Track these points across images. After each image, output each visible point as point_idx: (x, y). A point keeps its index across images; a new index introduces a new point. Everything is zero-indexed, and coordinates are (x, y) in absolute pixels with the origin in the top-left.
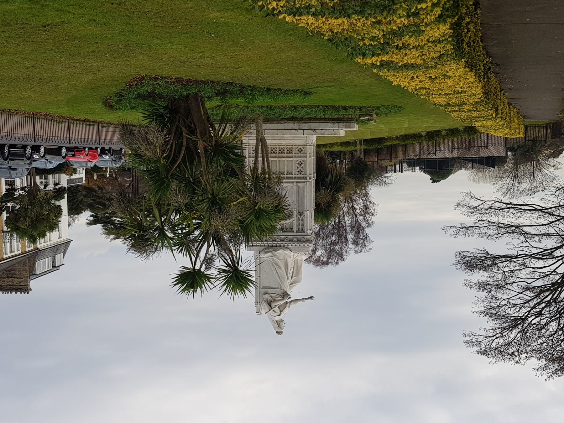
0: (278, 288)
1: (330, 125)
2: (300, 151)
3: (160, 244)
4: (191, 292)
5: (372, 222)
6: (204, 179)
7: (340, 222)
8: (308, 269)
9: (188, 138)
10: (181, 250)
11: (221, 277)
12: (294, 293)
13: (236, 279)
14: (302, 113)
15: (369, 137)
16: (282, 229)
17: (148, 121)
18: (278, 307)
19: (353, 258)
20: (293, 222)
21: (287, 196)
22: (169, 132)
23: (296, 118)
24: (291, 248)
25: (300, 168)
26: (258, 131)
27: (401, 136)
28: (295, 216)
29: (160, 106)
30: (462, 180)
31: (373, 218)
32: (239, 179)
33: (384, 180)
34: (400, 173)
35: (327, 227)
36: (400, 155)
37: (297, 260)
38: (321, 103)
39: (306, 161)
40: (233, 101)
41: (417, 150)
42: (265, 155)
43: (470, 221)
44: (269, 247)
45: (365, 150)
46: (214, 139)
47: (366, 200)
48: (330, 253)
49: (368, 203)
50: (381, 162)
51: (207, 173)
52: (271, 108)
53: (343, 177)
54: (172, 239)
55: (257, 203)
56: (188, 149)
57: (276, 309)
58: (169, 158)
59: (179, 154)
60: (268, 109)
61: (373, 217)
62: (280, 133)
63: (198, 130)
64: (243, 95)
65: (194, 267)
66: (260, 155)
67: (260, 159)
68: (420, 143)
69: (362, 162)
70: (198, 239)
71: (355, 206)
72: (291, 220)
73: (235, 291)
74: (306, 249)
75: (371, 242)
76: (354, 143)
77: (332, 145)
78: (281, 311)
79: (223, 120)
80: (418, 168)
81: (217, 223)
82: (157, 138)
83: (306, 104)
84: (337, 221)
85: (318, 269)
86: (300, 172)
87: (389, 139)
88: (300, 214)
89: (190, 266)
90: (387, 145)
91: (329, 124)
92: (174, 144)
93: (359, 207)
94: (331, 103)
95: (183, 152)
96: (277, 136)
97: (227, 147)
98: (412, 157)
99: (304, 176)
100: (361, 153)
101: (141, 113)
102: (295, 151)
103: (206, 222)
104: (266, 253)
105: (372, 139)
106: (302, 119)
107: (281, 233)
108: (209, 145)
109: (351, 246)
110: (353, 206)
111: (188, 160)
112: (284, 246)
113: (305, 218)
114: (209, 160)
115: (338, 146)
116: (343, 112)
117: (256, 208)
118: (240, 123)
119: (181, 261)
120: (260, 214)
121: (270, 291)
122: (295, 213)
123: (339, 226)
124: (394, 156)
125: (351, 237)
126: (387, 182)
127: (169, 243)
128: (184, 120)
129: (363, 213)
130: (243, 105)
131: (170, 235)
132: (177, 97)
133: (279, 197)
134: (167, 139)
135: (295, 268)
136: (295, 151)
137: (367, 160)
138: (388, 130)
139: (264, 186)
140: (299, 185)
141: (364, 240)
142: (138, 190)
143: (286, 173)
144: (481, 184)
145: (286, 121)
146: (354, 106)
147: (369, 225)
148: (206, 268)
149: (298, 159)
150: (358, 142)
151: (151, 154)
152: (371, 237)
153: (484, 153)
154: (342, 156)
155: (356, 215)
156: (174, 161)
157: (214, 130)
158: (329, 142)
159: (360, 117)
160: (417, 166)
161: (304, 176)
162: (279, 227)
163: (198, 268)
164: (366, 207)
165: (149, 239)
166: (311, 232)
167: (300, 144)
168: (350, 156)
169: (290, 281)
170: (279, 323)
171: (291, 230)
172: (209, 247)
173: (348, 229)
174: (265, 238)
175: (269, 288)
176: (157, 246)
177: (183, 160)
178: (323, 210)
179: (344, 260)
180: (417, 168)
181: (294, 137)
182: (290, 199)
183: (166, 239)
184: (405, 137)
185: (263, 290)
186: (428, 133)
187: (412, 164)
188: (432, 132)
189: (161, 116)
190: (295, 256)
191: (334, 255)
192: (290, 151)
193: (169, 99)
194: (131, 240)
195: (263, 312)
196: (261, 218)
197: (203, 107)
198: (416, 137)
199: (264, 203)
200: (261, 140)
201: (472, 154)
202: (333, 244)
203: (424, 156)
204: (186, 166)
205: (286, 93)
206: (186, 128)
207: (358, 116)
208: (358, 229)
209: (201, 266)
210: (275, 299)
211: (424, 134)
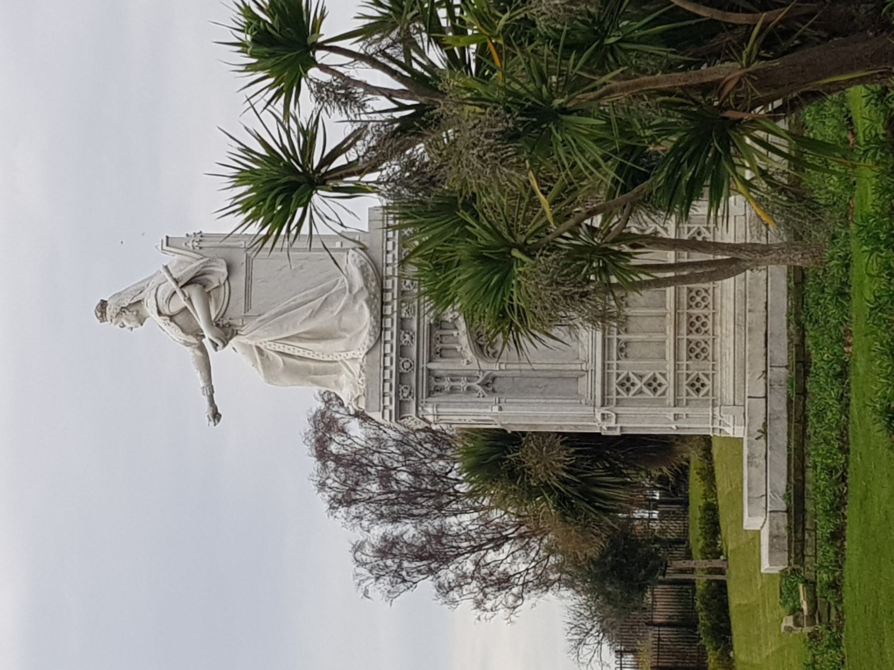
0: (248, 306)
1: (781, 484)
2: (696, 385)
4: (242, 36)
5: (454, 602)
6: (615, 83)
8: (307, 399)
9: (750, 27)
12: (232, 361)
13: (282, 185)
14: (823, 393)
15: (735, 600)
18: (185, 309)
19: (336, 539)
20: (465, 358)
21: (550, 342)
23: (807, 373)
24: (377, 354)
25: (639, 384)
26: (765, 250)
28: (484, 365)
31: (467, 604)
32: (611, 194)
33: (591, 640)
35: (441, 457)
37: (338, 371)
38: (855, 458)
39: (661, 403)
42: (685, 274)
44: (381, 280)
46: (746, 116)
47: (525, 584)
48: (354, 465)
49: (515, 590)
50: (651, 634)
51: (634, 93)
52: (842, 294)
55: (532, 257)
56: (713, 28)
57: (180, 302)
60: (837, 285)
62: (756, 318)
63: (777, 63)
65: (321, 46)
66: (685, 257)
67: (670, 257)
69: (654, 571)
71: (507, 547)
72: (469, 354)
73: (241, 178)
76: (713, 550)
77: (709, 475)
78: (171, 317)
81: (466, 122)
83: (854, 409)
86: (626, 384)
88: (489, 384)
90: (704, 655)
91: (784, 483)
94: (855, 492)
96: (744, 316)
97: (717, 157)
99: (614, 396)
100: (682, 571)
102: (697, 368)
103: (469, 90)
104: (363, 270)
106: (803, 393)
107: (428, 319)
108: (728, 96)
109: (380, 530)
110: (507, 538)
111: (675, 29)
112: (383, 329)
113: (474, 397)
114: (673, 99)
115: (705, 496)
116: (825, 528)
117: (516, 253)
118: (793, 200)
120: (496, 262)
121: (239, 281)
122: (491, 367)
123: (440, 494)
125: (408, 530)
126: (584, 650)
129: (484, 571)
130: (855, 202)
133: (545, 321)
135: (312, 364)
136: (697, 368)
138: (757, 661)
140: (583, 381)
141: (397, 574)
145: (796, 340)
146: (846, 567)
147: (444, 590)
148: (320, 86)
149: (671, 376)
150: (716, 564)
152: (406, 596)
154: (674, 508)
155: (480, 547)
157: (775, 116)
158: (717, 468)
159: (806, 582)
166: (430, 418)
167: (718, 383)
169: (269, 347)
171: (436, 353)
172: (389, 94)
173: (433, 525)
174: (412, 270)
175: (249, 279)
178: (499, 456)
179: (332, 507)
181: (741, 368)
182: (538, 353)
185: (240, 258)
190: (351, 364)
191: (349, 475)
192: (696, 352)
195: (171, 259)
196: (478, 257)
199: (529, 278)
200: (734, 261)
202: (386, 476)
204: (657, 21)
206: (781, 21)
208: (434, 554)
209: (324, 68)
210: (209, 299)
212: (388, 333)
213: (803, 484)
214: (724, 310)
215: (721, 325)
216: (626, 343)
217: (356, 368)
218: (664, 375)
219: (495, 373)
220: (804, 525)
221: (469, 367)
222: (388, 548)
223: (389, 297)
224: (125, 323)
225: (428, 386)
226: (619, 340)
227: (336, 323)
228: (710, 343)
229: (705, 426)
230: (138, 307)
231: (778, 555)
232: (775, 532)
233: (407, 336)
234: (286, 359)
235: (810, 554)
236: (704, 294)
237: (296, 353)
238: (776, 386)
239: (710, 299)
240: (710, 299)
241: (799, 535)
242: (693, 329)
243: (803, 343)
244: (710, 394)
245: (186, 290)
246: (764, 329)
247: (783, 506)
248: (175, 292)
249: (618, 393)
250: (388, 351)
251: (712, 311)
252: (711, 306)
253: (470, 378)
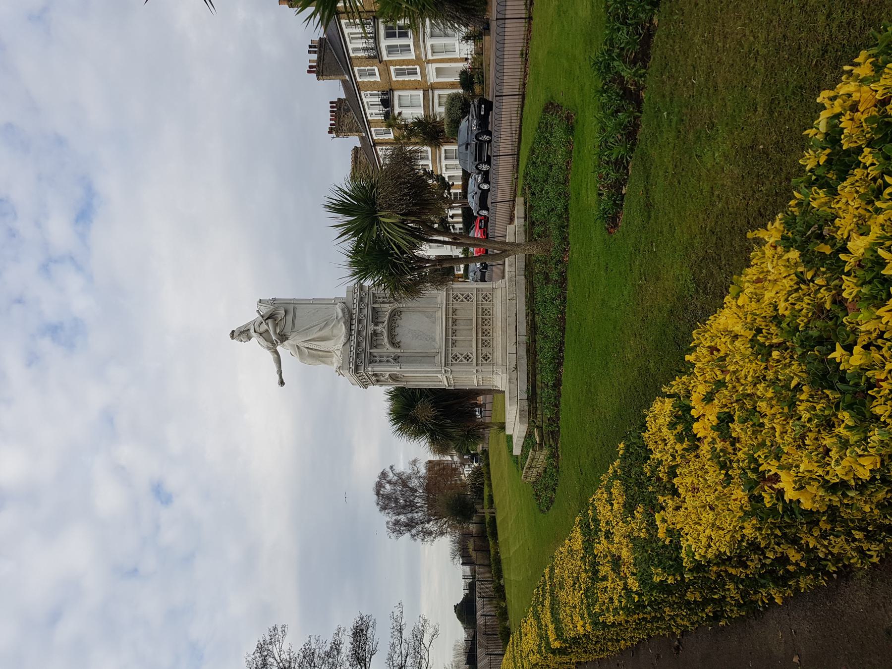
0: (293, 327)
2: (485, 358)
15: (498, 522)
24: (348, 346)
30: (455, 634)
31: (419, 540)
37: (332, 357)
39: (470, 365)
43: (407, 634)
50: (472, 540)
57: (264, 327)
72: (388, 346)
75: (397, 537)
77: (490, 486)
78: (261, 334)
85: (373, 485)
86: (455, 357)
88: (396, 359)
93: (431, 526)
102: (486, 351)
104: (343, 310)
106: (534, 341)
109: (394, 518)
112: (351, 335)
121: (290, 318)
124: (479, 553)
125: (403, 518)
135: (321, 353)
136: (486, 351)
140: (437, 358)
143: (454, 338)
144: (453, 653)
145: (530, 318)
147: (413, 536)
149: (475, 354)
153: (480, 652)
164: (430, 533)
173: (410, 516)
175: (294, 316)
180: (467, 592)
184: (498, 561)
186: (503, 586)
187: (472, 587)
188: (503, 591)
192: (485, 344)
198: (499, 574)
201: (480, 639)
208: (410, 525)
211: (502, 582)
217: (339, 353)
222: (397, 523)
223: (354, 322)
247: (525, 396)
253: (388, 356)
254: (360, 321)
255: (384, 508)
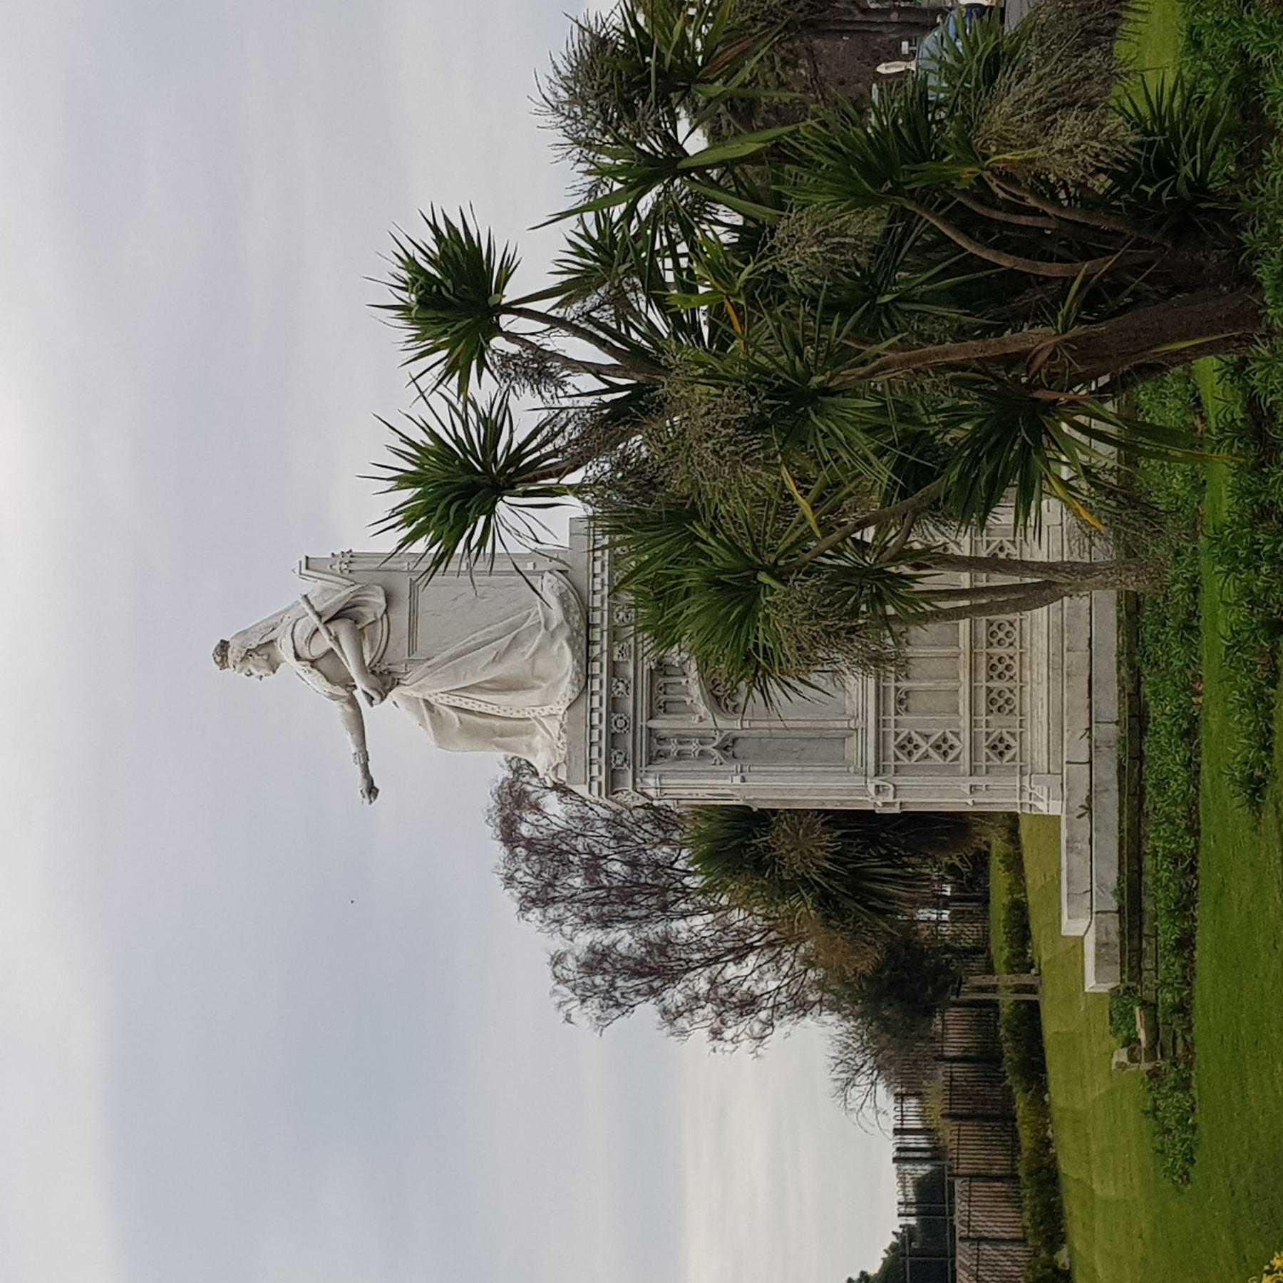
0: (412, 648)
1: (1112, 877)
2: (999, 747)
3: (608, 160)
4: (404, 295)
5: (683, 1032)
6: (891, 355)
7: (685, 892)
9: (1067, 281)
10: (582, 252)
11: (465, 425)
12: (392, 719)
13: (457, 488)
14: (1165, 757)
15: (1051, 1026)
16: (662, 668)
17: (1144, 109)
19: (530, 949)
20: (696, 713)
22: (1089, 201)
24: (582, 709)
25: (925, 747)
26: (1088, 570)
27: (1054, 1160)
28: (721, 723)
29: (1208, 161)
31: (701, 1034)
33: (862, 1080)
34: (891, 1152)
35: (664, 841)
36: (968, 1149)
37: (531, 732)
38: (1208, 843)
39: (953, 770)
40: (1223, 474)
41: (998, 1231)
42: (983, 603)
44: (587, 611)
45: (994, 1004)
47: (776, 1007)
48: (552, 852)
49: (763, 1015)
51: (919, 368)
53: (888, 924)
54: (630, 213)
55: (784, 582)
56: (1017, 282)
57: (323, 643)
58: (980, 200)
59: (995, 246)
61: (704, 1034)
63: (1102, 328)
64: (1248, 514)
65: (508, 309)
68: (1022, 1241)
70: (628, 324)
71: (751, 960)
72: (703, 709)
74: (580, 772)
75: (601, 1022)
76: (1022, 961)
77: (1015, 864)
78: (313, 663)
79: (1137, 439)
80: (912, 1221)
81: (695, 406)
82: (1070, 151)
83: (1205, 778)
84: (687, 881)
86: (907, 746)
87: (1042, 1109)
88: (728, 747)
89: (511, 293)
90: (1010, 1100)
92: (1039, 222)
93: (744, 973)
95: (1006, 262)
96: (1061, 661)
98: (960, 1205)
99: (892, 762)
101: (1179, 76)
103: (702, 365)
104: (562, 599)
105: (1039, 1035)
107: (648, 664)
109: (586, 938)
110: (751, 948)
112: (589, 676)
113: (708, 765)
114: (966, 376)
115: (1011, 891)
116: (1168, 933)
117: (763, 577)
118: (1123, 504)
119: (536, 259)
120: (737, 592)
121: (400, 616)
122: (732, 725)
123: (664, 890)
124: (968, 1127)
125: (623, 939)
126: (854, 1093)
127: (613, 199)
128: (1147, 265)
130: (1205, 509)
131: (645, 204)
132: (1246, 236)
134: (1062, 195)
135: (497, 723)
136: (999, 725)
137: (951, 1013)
139: (855, 613)
140: (851, 743)
141: (608, 995)
142: (822, 33)
143: (904, 685)
145: (1129, 687)
147: (670, 1016)
149: (965, 736)
150: (1026, 979)
151: (998, 125)
152: (622, 1024)
154: (971, 906)
155: (716, 960)
156: (967, 223)
159: (1144, 1004)
160: (922, 1222)
161: (892, 763)
162: (674, 656)
163: (502, 324)
164: (748, 1005)
165: (633, 117)
166: (652, 792)
168: (967, 942)
169: (440, 700)
170: (262, 652)
171: (659, 707)
172: (597, 370)
173: (654, 931)
175: (413, 613)
176: (601, 149)
177: (971, 263)
178: (742, 843)
179: (524, 910)
182: (789, 707)
183: (629, 187)
184: (1048, 1178)
187: (931, 1200)
189: (1163, 167)
190: (548, 722)
191: (545, 866)
192: (998, 703)
193: (1236, 199)
194: (626, 35)
195: (313, 587)
196: (713, 581)
197: (1200, 346)
198: (1050, 1226)
199: (782, 610)
202: (593, 866)
203: (963, 1255)
205: (1260, 703)
207: (1148, 995)
208: (656, 969)
209: (512, 337)
210: (362, 636)
211: (1062, 1257)
212: (596, 682)
213: (1140, 875)
214: (1035, 650)
215: (1031, 669)
216: (906, 693)
217: (554, 727)
218: (956, 734)
219: (737, 734)
220: (1141, 929)
221: (702, 725)
222: (597, 961)
224: (253, 670)
225: (649, 750)
226: (897, 689)
227: (528, 668)
228: (1017, 691)
229: (1012, 800)
230: (268, 650)
231: (1107, 968)
232: (1104, 939)
233: (620, 684)
234: (464, 716)
235: (1149, 967)
236: (1008, 628)
237: (477, 709)
238: (1104, 749)
239: (1016, 634)
240: (1016, 634)
241: (1136, 942)
242: (995, 674)
243: (1138, 692)
244: (1018, 758)
245: (332, 627)
246: (1088, 673)
247: (1114, 905)
248: (317, 630)
249: (897, 759)
250: (596, 704)
251: (1018, 730)
252: (1017, 644)
254: (614, 634)
255: (540, 898)
